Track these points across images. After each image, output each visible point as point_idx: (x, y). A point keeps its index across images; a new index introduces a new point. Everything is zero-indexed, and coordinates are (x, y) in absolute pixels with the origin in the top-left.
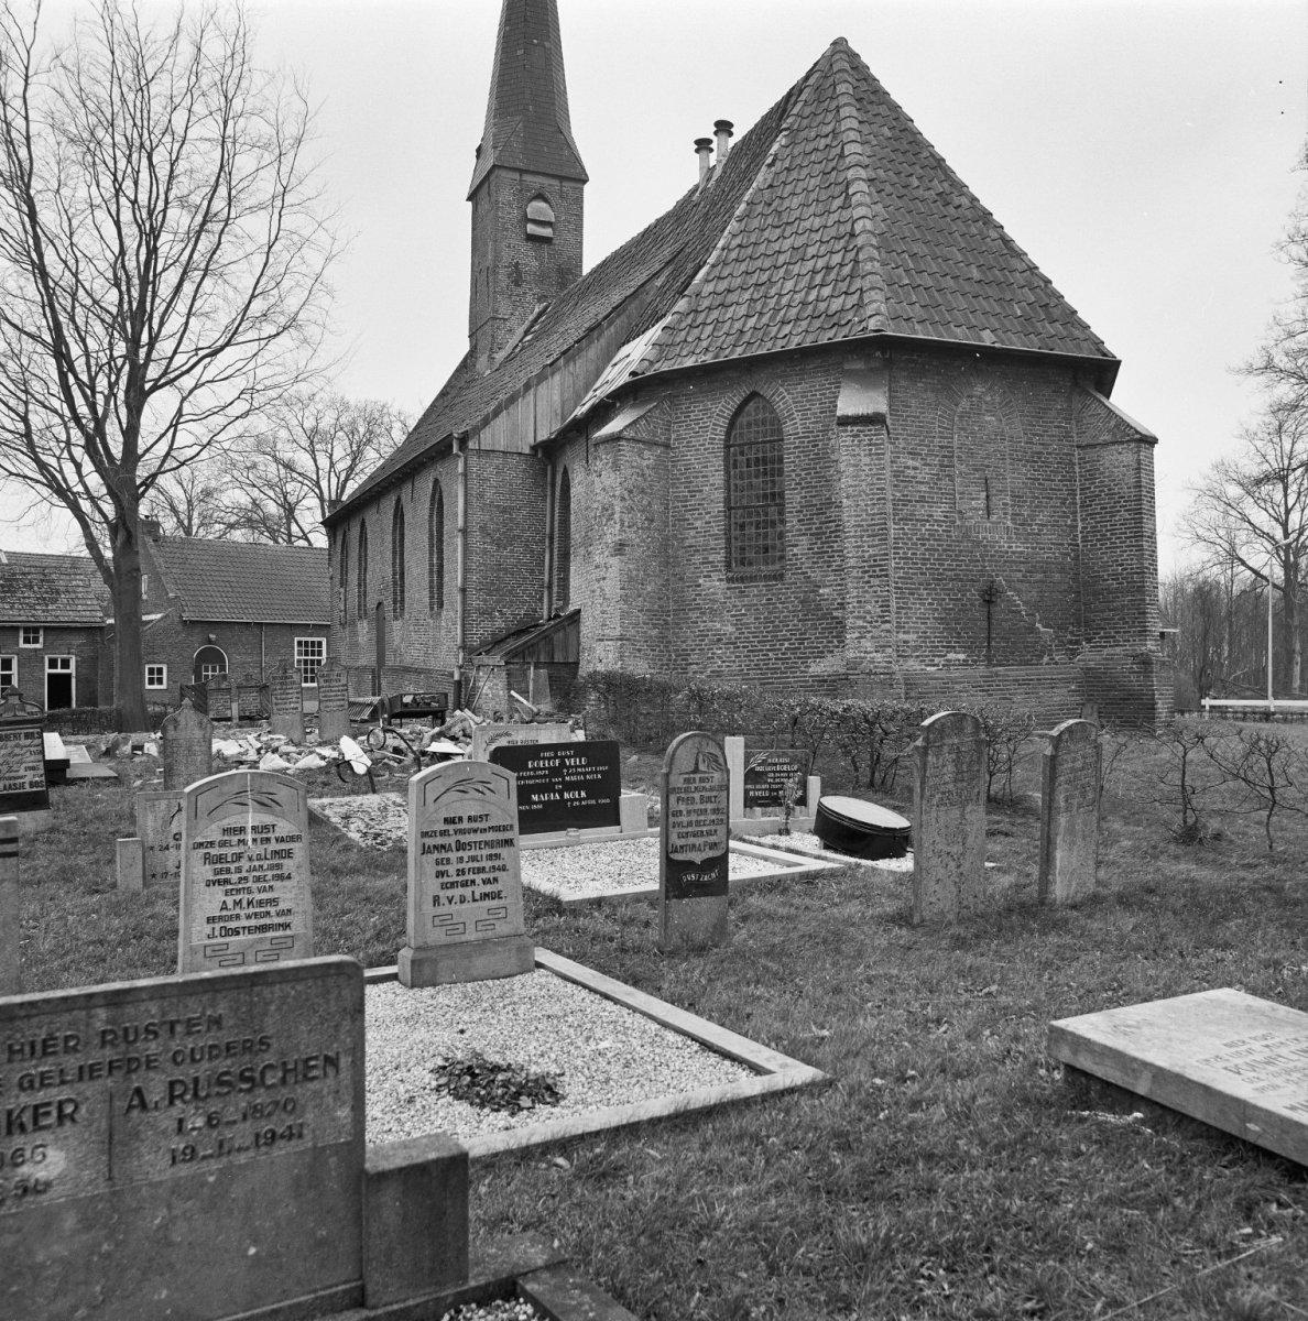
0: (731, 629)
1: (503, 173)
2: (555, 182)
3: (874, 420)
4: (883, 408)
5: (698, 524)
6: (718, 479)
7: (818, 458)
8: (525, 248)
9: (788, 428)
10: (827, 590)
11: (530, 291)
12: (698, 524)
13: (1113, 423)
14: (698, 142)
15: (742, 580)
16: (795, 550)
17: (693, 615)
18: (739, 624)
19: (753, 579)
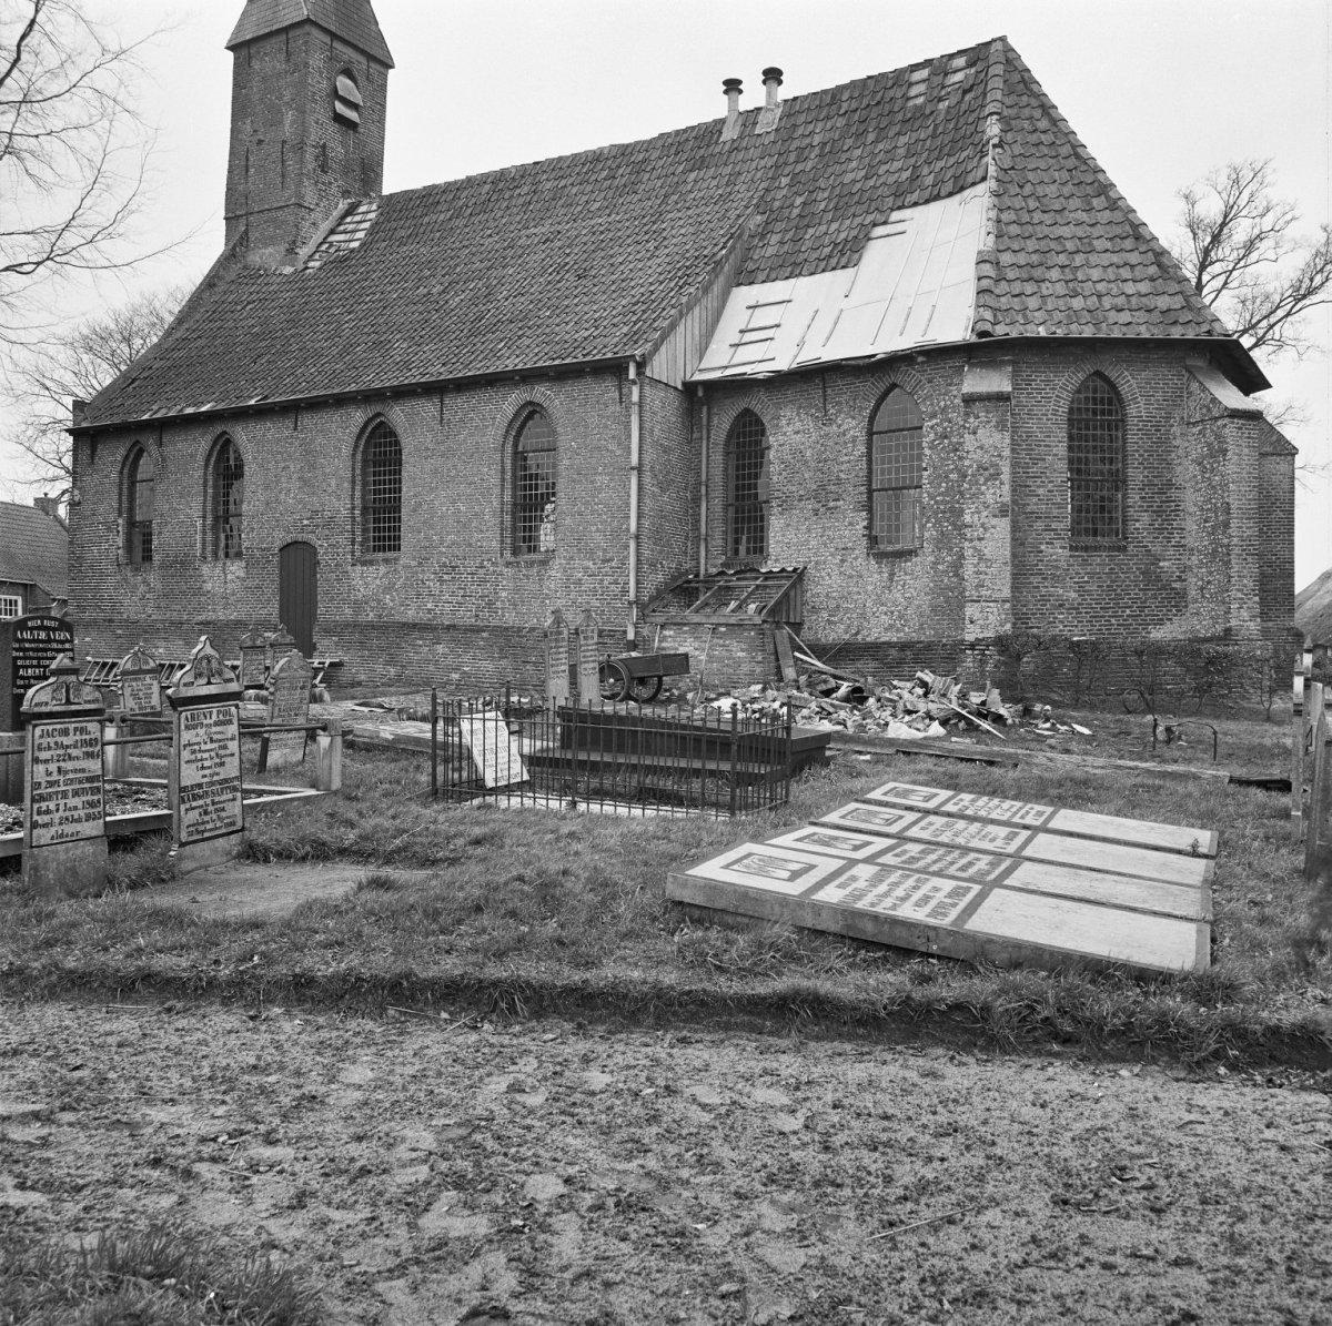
0: (1074, 595)
1: (315, 32)
2: (362, 59)
3: (1001, 398)
4: (1007, 387)
5: (1041, 491)
6: (1061, 449)
7: (1160, 442)
8: (333, 128)
9: (1132, 410)
10: (1166, 564)
11: (336, 182)
12: (1041, 491)
13: (1274, 438)
14: (766, 72)
15: (1086, 549)
16: (1137, 525)
17: (1035, 580)
18: (1081, 590)
19: (1096, 549)
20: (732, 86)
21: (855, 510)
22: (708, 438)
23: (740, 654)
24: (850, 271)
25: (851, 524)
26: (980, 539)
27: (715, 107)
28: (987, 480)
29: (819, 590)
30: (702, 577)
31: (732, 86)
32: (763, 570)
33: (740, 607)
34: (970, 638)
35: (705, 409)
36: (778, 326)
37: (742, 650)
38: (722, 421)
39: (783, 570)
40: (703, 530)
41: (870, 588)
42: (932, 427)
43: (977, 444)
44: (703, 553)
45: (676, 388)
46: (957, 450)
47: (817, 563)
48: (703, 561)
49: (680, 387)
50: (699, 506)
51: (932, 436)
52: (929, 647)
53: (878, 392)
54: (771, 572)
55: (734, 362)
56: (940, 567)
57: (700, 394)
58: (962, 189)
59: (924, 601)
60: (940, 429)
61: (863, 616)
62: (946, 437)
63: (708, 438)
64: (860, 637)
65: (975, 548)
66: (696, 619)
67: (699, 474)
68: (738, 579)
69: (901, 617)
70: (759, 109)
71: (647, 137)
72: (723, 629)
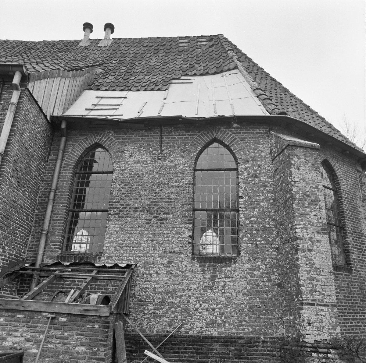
20: (88, 27)
21: (182, 222)
22: (62, 159)
23: (79, 349)
24: (161, 94)
25: (178, 233)
26: (310, 250)
27: (76, 34)
28: (310, 204)
29: (147, 285)
30: (37, 266)
31: (88, 27)
32: (97, 265)
33: (81, 296)
34: (309, 339)
35: (63, 139)
36: (119, 105)
37: (82, 345)
38: (75, 150)
39: (116, 266)
40: (46, 227)
41: (194, 286)
42: (245, 169)
43: (301, 177)
44: (42, 245)
45: (45, 116)
46: (265, 186)
47: (146, 262)
48: (41, 252)
49: (48, 118)
50: (45, 209)
51: (246, 175)
52: (250, 342)
53: (203, 143)
54: (104, 266)
55: (89, 114)
56: (256, 273)
57: (63, 126)
58: (222, 71)
59: (243, 301)
60: (252, 171)
61: (186, 311)
62: (256, 177)
63: (62, 159)
64: (183, 330)
65: (306, 257)
66: (34, 306)
67: (49, 184)
68: (72, 271)
69: (221, 314)
70: (101, 40)
71: (37, 40)
72: (63, 319)
